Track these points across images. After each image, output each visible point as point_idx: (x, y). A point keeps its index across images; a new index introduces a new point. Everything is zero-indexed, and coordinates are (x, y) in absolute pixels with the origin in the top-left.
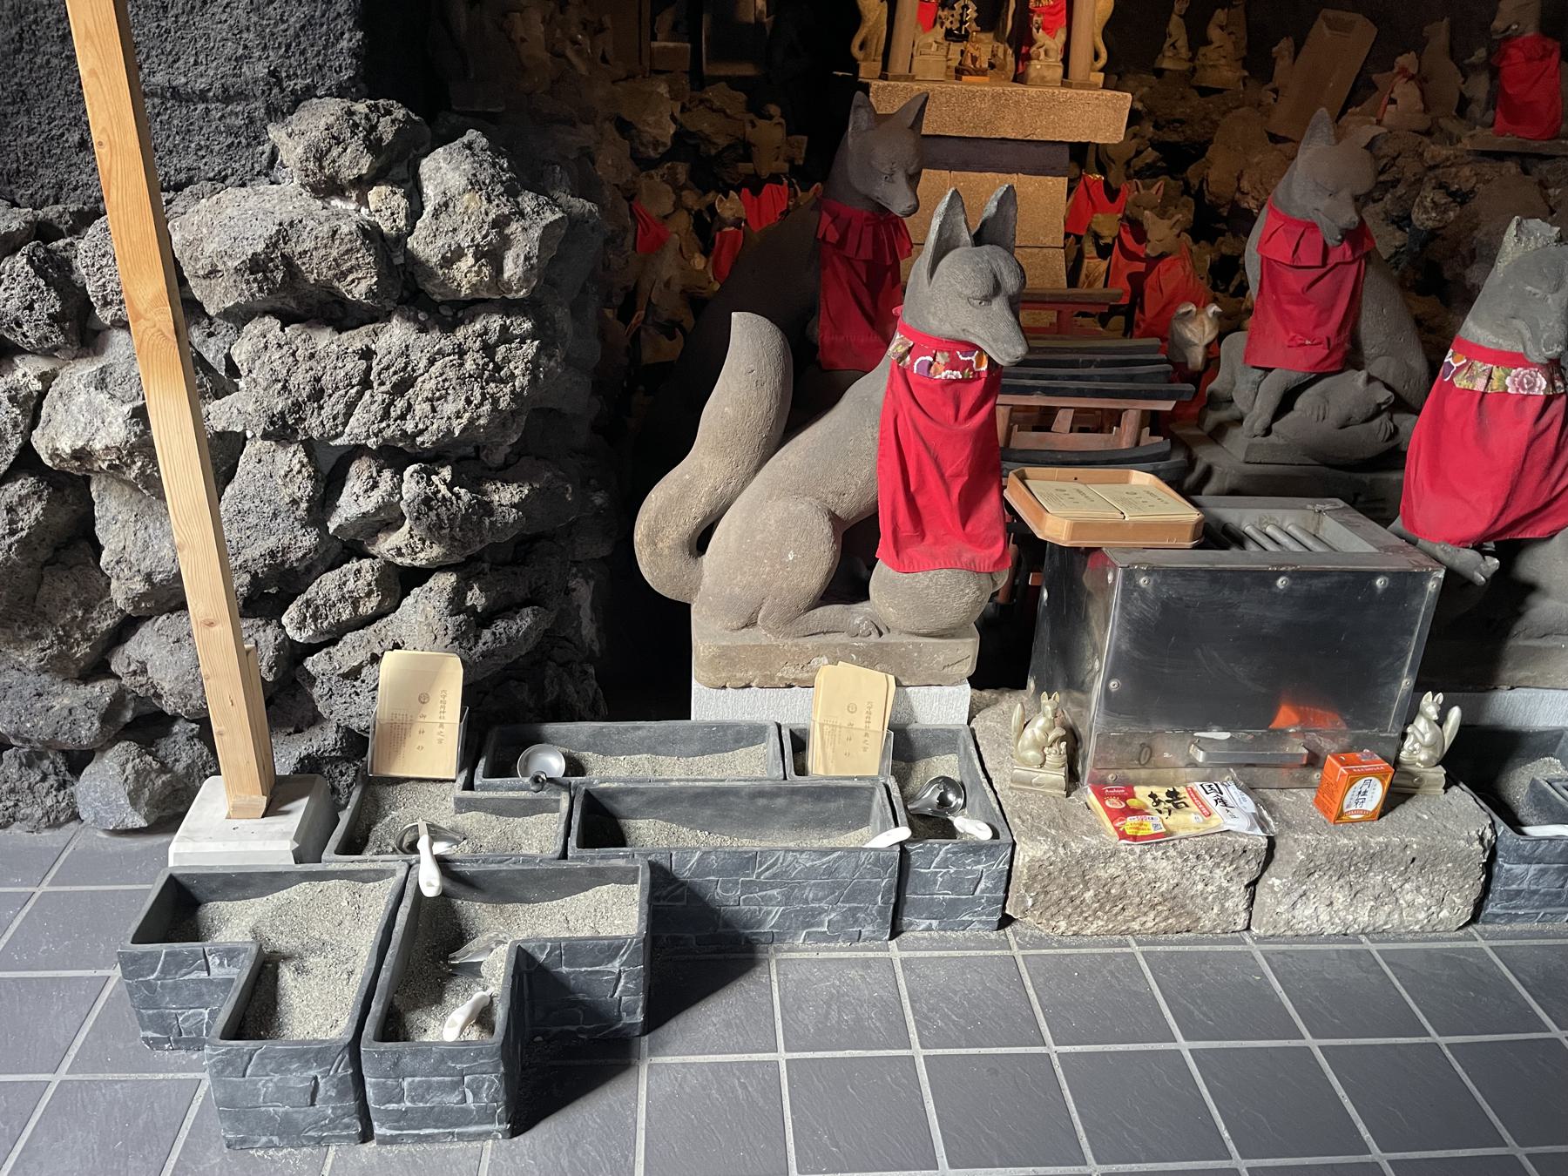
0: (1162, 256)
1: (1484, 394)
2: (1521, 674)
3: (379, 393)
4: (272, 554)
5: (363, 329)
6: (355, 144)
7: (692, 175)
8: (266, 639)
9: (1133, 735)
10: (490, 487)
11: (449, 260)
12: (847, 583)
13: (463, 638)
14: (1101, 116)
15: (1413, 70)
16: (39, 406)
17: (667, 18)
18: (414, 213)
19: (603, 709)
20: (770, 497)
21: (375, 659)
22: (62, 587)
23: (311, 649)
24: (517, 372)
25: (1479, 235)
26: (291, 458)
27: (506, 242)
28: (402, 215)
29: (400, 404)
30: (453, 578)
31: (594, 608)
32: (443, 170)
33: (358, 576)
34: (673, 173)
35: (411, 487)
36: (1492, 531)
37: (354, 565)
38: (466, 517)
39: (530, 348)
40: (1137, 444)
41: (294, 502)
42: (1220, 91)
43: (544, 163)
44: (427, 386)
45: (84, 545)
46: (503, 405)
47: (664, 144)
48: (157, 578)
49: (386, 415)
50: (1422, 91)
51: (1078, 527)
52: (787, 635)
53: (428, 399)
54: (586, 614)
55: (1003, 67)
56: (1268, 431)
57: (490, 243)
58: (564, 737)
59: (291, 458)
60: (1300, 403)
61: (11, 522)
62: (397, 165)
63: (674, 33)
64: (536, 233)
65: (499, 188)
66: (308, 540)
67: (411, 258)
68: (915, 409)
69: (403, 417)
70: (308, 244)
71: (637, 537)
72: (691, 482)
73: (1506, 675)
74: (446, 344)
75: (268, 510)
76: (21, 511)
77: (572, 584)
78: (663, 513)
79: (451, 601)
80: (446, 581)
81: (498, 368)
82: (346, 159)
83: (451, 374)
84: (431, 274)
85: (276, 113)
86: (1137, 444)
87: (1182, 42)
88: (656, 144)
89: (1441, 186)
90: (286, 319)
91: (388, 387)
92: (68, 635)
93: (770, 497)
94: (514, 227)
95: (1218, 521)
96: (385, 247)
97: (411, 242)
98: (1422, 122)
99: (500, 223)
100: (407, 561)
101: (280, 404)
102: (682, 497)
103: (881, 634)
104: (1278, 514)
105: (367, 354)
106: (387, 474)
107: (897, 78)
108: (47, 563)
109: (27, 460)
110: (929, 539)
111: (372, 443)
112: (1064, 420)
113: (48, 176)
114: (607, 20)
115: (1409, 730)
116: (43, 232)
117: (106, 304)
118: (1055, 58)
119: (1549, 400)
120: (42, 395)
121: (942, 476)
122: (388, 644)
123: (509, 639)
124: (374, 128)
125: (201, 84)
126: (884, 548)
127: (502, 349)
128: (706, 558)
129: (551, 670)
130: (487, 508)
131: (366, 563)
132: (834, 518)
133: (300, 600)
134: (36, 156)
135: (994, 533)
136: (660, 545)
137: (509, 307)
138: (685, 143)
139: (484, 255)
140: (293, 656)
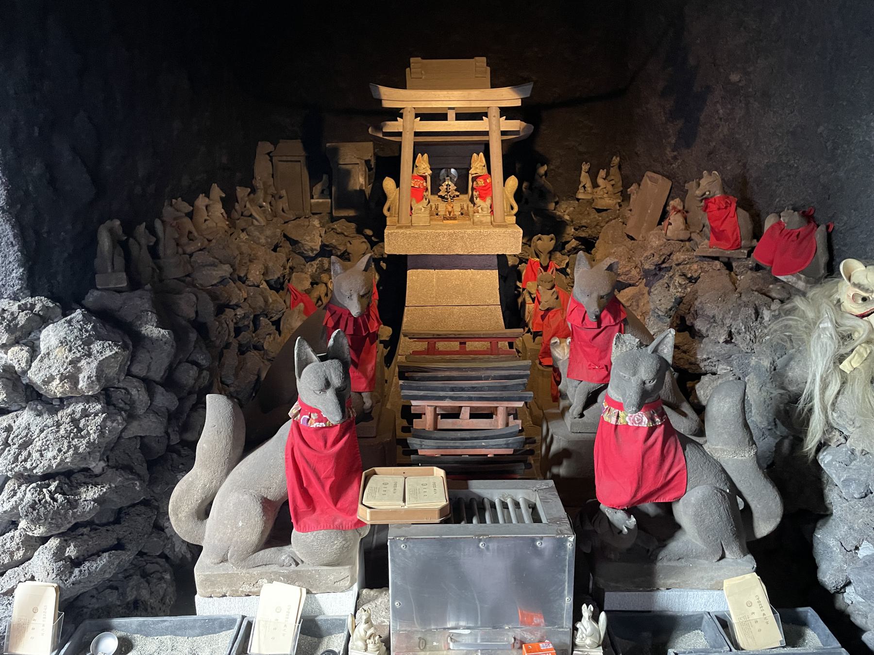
0: (548, 310)
1: (616, 426)
2: (670, 582)
3: (14, 449)
10: (83, 490)
14: (509, 240)
15: (680, 208)
17: (318, 188)
20: (231, 491)
24: (91, 432)
25: (697, 303)
27: (79, 370)
28: (24, 361)
29: (25, 454)
32: (50, 337)
39: (99, 420)
40: (507, 425)
42: (606, 210)
43: (142, 311)
44: (38, 444)
46: (81, 450)
47: (316, 250)
49: (16, 459)
50: (686, 219)
52: (243, 567)
53: (38, 451)
56: (582, 415)
57: (69, 372)
58: (124, 626)
62: (25, 336)
63: (322, 194)
64: (95, 364)
68: (301, 444)
69: (25, 460)
72: (192, 482)
73: (661, 581)
74: (50, 422)
78: (180, 499)
79: (55, 554)
80: (53, 543)
81: (80, 430)
83: (51, 437)
86: (507, 425)
87: (589, 185)
88: (312, 250)
91: (16, 446)
93: (231, 491)
94: (83, 362)
95: (479, 497)
97: (29, 374)
98: (684, 235)
99: (74, 362)
102: (188, 490)
103: (297, 564)
104: (512, 492)
105: (9, 429)
110: (318, 511)
112: (465, 413)
114: (283, 193)
115: (578, 625)
118: (487, 211)
119: (651, 430)
121: (319, 479)
122: (28, 576)
123: (90, 573)
124: (15, 318)
128: (209, 520)
136: (180, 515)
139: (66, 378)
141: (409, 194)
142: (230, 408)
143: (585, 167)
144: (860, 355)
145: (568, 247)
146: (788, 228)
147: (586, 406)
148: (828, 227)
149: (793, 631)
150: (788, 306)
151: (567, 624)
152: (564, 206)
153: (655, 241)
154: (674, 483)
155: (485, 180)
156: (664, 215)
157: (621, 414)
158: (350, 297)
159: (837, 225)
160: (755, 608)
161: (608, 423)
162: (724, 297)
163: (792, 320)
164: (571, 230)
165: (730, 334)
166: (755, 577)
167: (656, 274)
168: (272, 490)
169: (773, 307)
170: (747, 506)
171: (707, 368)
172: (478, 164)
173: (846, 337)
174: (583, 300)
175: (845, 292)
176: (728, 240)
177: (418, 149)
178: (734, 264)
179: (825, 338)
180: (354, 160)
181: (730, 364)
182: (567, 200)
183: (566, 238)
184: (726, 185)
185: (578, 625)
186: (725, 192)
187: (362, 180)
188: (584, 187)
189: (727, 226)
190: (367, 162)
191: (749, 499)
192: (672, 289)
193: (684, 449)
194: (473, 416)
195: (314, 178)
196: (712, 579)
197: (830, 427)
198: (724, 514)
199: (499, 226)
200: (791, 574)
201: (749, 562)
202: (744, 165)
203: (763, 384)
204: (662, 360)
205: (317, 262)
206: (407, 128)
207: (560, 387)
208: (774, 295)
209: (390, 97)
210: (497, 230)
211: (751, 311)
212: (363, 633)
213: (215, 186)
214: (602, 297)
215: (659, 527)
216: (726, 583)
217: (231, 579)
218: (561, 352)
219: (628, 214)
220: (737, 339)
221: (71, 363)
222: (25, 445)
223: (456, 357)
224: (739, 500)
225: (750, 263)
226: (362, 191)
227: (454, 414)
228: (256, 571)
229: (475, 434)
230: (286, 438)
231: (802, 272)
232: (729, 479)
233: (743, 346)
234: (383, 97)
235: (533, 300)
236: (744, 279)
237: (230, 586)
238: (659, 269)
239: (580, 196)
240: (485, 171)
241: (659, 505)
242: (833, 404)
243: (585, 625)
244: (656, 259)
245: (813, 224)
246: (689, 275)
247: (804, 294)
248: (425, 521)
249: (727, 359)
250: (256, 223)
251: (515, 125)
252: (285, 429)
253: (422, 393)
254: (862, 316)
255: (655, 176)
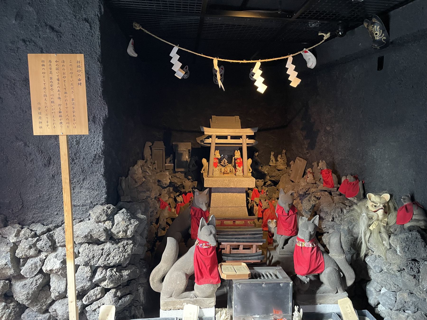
0: (265, 209)
2: (321, 301)
3: (104, 256)
4: (82, 287)
5: (102, 245)
6: (104, 215)
7: (173, 190)
8: (80, 303)
9: (241, 317)
10: (123, 271)
11: (118, 233)
12: (190, 287)
13: (116, 302)
14: (250, 182)
15: (311, 171)
16: (44, 262)
18: (113, 225)
19: (144, 316)
21: (99, 307)
22: (43, 295)
23: (87, 306)
25: (321, 207)
26: (88, 269)
27: (128, 229)
29: (108, 258)
30: (115, 290)
31: (143, 293)
32: (118, 218)
33: (98, 290)
34: (169, 190)
35: (108, 273)
36: (309, 272)
37: (97, 288)
38: (118, 278)
40: (257, 252)
41: (87, 277)
45: (47, 286)
46: (126, 257)
48: (60, 293)
49: (105, 260)
51: (227, 276)
52: (178, 299)
54: (142, 295)
55: (232, 172)
56: (283, 248)
59: (88, 269)
60: (289, 242)
61: (36, 283)
62: (110, 218)
64: (133, 227)
65: (128, 220)
66: (89, 284)
67: (112, 233)
68: (200, 254)
69: (108, 260)
70: (95, 233)
71: (150, 280)
73: (318, 301)
74: (117, 247)
75: (82, 279)
76: (38, 281)
77: (139, 289)
78: (155, 275)
79: (114, 295)
80: (113, 291)
81: (125, 250)
82: (102, 218)
84: (115, 235)
85: (91, 208)
86: (257, 252)
87: (274, 160)
88: (166, 184)
89: (315, 197)
90: (89, 243)
92: (42, 304)
94: (130, 226)
95: (258, 272)
96: (106, 230)
97: (112, 230)
98: (313, 182)
99: (127, 226)
100: (106, 287)
101: (87, 259)
102: (158, 271)
104: (269, 270)
106: (104, 270)
107: (210, 177)
108: (41, 290)
109: (41, 271)
110: (204, 278)
111: (102, 265)
112: (241, 247)
113: (50, 219)
114: (156, 162)
115: (294, 313)
116: (49, 230)
117: (59, 243)
118: (241, 171)
119: (313, 248)
120: (45, 259)
122: (102, 304)
125: (79, 204)
126: (196, 281)
127: (126, 246)
129: (133, 308)
130: (122, 276)
131: (99, 288)
132: (186, 275)
133: (86, 296)
134: (48, 216)
135: (216, 276)
137: (128, 239)
138: (171, 184)
140: (84, 307)
141: (213, 164)
142: (175, 242)
143: (272, 153)
144: (375, 224)
145: (267, 184)
146: (350, 182)
147: (284, 245)
148: (362, 182)
149: (361, 316)
150: (352, 208)
151: (290, 313)
152: (265, 168)
153: (303, 184)
154: (320, 267)
155: (240, 160)
156: (305, 173)
157: (303, 243)
158: (202, 204)
159: (365, 181)
160: (349, 309)
161: (299, 246)
162: (330, 205)
163: (353, 213)
164: (268, 177)
165: (333, 218)
166: (348, 299)
167: (304, 196)
168: (189, 271)
169: (347, 208)
170: (344, 275)
171: (326, 231)
172: (237, 154)
173: (371, 219)
174: (283, 205)
175: (369, 204)
176: (329, 184)
177: (216, 148)
178: (332, 193)
179: (364, 219)
180: (184, 150)
181: (334, 229)
182: (266, 165)
183: (267, 180)
184: (327, 164)
185: (294, 313)
186: (327, 167)
187: (187, 157)
189: (329, 180)
190: (189, 150)
191: (344, 272)
192: (311, 202)
193: (323, 255)
194: (244, 249)
195: (167, 155)
196: (334, 300)
197: (368, 249)
198: (337, 277)
199: (246, 177)
200: (359, 297)
201: (346, 294)
202: (333, 158)
203: (346, 235)
204: (315, 225)
206: (213, 142)
207: (273, 238)
208: (347, 204)
209: (207, 131)
210: (246, 179)
211: (340, 210)
212: (224, 318)
214: (290, 205)
215: (317, 283)
216: (339, 301)
217: (174, 303)
218: (272, 225)
219: (291, 172)
220: (336, 220)
221: (126, 226)
222: (108, 255)
223: (232, 227)
224: (341, 274)
225: (338, 193)
226: (187, 161)
227: (237, 248)
228: (182, 300)
229: (246, 255)
230: (194, 251)
231: (355, 197)
232: (337, 265)
233: (338, 222)
234: (205, 131)
235: (257, 205)
236: (336, 198)
237: (173, 306)
238: (306, 194)
239: (271, 164)
240: (240, 157)
241: (315, 276)
242: (368, 241)
243: (296, 313)
244: (304, 190)
245: (358, 180)
247: (356, 204)
248: (244, 278)
249: (333, 227)
251: (252, 141)
252: (192, 249)
253: (226, 240)
254: (375, 212)
255: (301, 159)
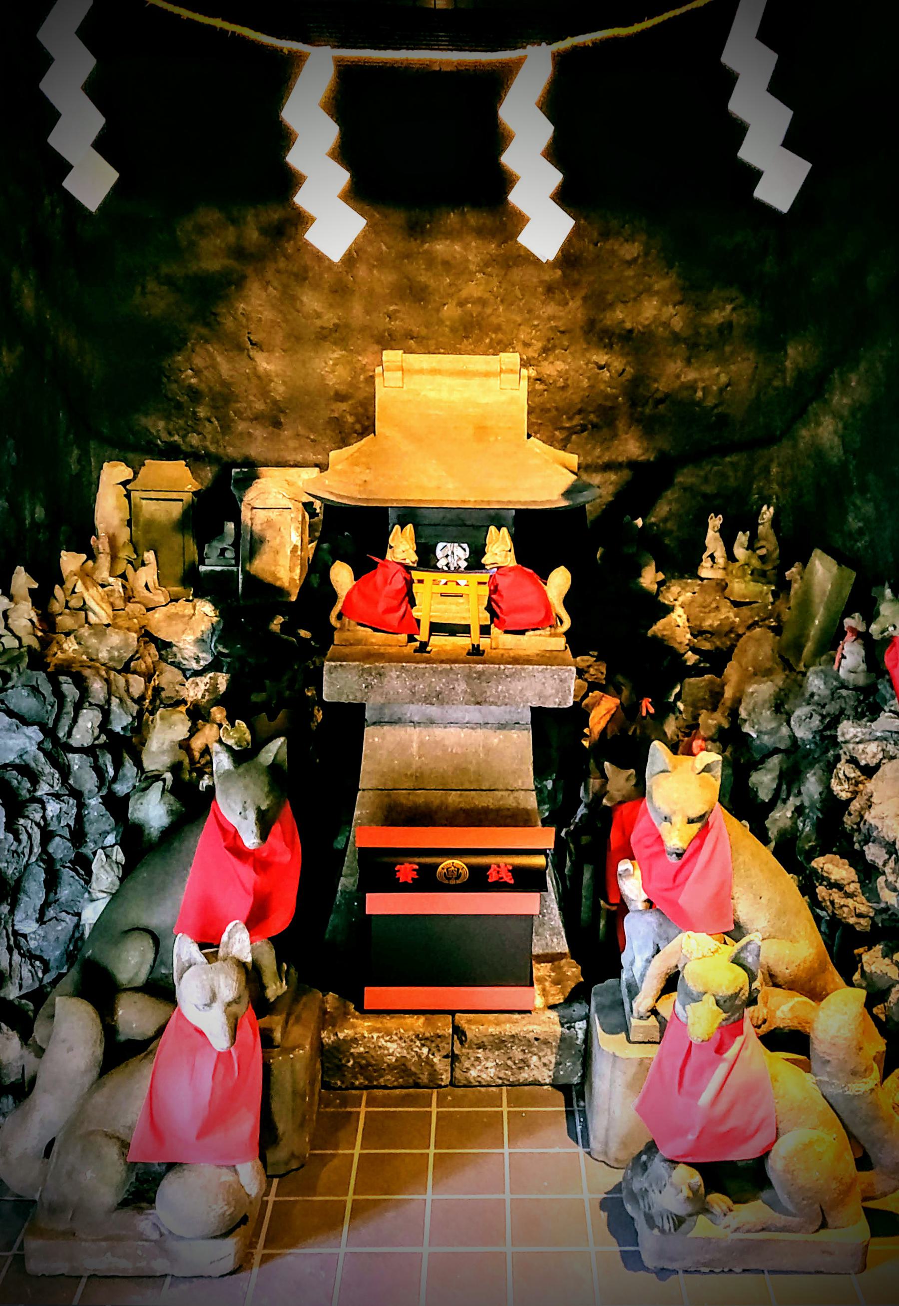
143: (715, 522)
182: (682, 577)
188: (712, 557)
205: (206, 679)
213: (20, 570)
246: (863, 763)
250: (93, 618)
